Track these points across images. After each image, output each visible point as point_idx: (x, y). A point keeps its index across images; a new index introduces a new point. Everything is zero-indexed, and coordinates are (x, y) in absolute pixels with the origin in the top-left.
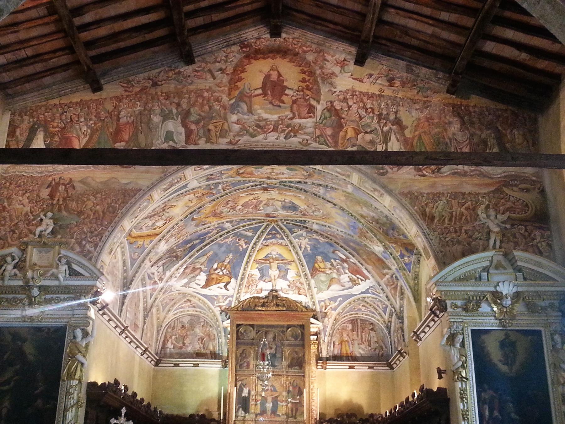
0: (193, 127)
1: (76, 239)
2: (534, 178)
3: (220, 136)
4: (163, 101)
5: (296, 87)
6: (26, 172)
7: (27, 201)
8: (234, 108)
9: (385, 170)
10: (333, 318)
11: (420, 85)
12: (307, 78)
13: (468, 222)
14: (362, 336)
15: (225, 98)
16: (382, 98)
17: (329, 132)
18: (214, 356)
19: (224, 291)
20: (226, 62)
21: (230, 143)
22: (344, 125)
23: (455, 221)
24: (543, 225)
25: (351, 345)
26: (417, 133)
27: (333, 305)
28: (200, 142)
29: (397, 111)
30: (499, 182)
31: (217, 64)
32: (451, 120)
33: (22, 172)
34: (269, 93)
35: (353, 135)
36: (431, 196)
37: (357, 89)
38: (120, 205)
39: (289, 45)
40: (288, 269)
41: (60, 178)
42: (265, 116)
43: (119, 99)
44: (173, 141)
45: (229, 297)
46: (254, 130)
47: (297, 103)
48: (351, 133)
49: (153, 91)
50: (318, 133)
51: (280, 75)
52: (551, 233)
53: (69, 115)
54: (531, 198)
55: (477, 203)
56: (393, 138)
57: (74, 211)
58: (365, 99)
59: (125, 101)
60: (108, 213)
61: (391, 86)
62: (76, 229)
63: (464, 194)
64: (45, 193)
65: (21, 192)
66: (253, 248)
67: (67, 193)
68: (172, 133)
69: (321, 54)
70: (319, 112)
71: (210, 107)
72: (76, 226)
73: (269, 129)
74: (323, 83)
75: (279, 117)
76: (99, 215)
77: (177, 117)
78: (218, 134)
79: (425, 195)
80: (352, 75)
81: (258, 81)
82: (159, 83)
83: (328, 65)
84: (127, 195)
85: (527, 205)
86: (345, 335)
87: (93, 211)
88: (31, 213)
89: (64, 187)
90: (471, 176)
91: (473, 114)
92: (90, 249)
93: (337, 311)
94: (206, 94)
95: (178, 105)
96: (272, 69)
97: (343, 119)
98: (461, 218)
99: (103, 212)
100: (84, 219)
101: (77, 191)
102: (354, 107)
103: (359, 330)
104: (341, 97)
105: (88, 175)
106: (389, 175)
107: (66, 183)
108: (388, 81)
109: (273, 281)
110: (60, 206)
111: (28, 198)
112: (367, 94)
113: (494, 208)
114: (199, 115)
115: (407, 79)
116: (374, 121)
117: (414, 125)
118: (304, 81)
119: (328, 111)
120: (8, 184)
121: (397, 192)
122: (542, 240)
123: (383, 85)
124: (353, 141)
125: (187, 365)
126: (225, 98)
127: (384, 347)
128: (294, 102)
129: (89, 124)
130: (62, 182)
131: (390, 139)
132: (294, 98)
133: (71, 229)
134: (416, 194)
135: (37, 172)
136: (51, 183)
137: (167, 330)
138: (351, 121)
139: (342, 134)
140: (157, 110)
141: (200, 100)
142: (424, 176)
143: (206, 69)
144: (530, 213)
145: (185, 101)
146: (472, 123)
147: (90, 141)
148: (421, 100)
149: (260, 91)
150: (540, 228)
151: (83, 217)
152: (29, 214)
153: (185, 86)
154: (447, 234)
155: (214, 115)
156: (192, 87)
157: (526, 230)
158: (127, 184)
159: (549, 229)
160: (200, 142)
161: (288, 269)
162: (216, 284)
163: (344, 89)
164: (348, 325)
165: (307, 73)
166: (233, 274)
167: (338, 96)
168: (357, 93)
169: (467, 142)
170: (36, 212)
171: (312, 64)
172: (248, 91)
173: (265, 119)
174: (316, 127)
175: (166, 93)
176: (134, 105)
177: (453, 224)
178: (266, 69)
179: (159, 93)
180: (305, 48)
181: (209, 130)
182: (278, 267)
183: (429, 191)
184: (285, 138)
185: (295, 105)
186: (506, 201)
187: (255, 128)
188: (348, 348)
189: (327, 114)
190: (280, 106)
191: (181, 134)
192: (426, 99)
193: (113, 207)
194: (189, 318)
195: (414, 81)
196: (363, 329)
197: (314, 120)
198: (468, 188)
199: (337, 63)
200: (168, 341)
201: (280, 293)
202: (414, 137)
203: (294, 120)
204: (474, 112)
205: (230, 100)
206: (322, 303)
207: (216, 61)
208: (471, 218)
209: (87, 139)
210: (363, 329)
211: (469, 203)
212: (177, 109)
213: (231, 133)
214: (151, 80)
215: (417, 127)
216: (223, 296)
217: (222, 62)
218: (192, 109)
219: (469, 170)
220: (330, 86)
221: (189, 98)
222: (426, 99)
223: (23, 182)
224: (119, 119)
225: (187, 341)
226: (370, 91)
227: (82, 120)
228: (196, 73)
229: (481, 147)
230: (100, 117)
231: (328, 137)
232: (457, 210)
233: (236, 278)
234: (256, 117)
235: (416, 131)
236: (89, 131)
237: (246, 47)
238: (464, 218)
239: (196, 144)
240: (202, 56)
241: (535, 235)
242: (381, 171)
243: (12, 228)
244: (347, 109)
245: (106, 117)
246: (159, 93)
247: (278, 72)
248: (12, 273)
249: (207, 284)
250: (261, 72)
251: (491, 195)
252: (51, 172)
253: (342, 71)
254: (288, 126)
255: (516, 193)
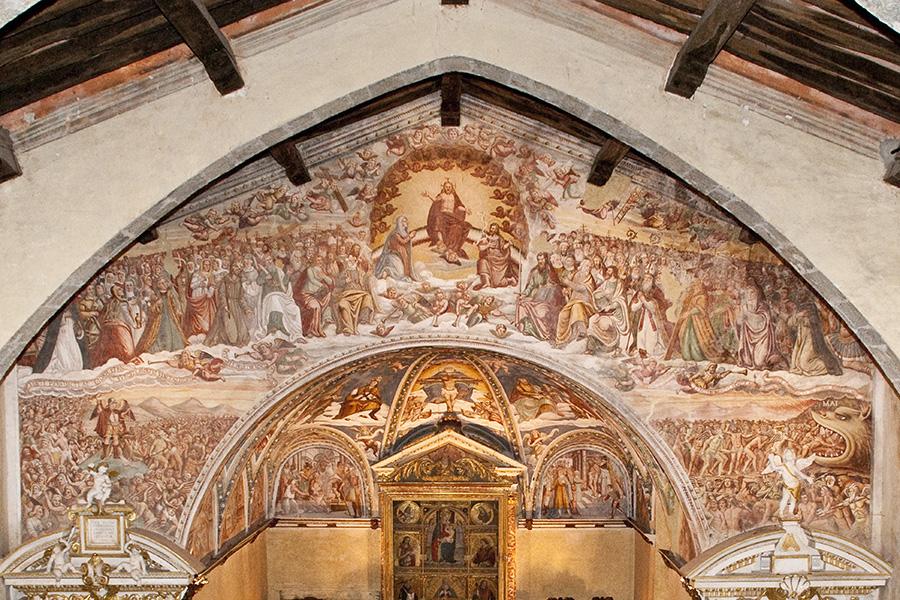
0: (314, 304)
1: (147, 503)
2: (859, 397)
3: (359, 321)
4: (261, 256)
5: (486, 228)
6: (56, 392)
7: (65, 440)
8: (380, 266)
9: (630, 382)
10: (545, 453)
11: (696, 225)
12: (506, 208)
13: (752, 471)
14: (588, 476)
15: (365, 249)
16: (632, 249)
17: (541, 312)
18: (358, 511)
19: (370, 421)
20: (364, 176)
21: (378, 333)
22: (567, 298)
23: (734, 468)
24: (862, 475)
25: (570, 491)
26: (686, 314)
27: (544, 437)
28: (327, 331)
29: (656, 274)
30: (808, 403)
31: (349, 181)
32: (742, 291)
33: (49, 391)
34: (440, 236)
35: (582, 318)
36: (700, 427)
37: (590, 230)
38: (207, 446)
39: (474, 142)
40: (473, 389)
41: (110, 400)
42: (435, 282)
43: (185, 253)
44: (282, 330)
45: (378, 428)
46: (417, 309)
47: (489, 256)
48: (577, 314)
49: (241, 236)
50: (523, 314)
51: (458, 203)
52: (872, 487)
53: (108, 285)
54: (851, 430)
55: (769, 438)
56: (647, 322)
57: (138, 456)
58: (603, 250)
59: (197, 257)
60: (190, 459)
61: (648, 225)
62: (145, 485)
63: (751, 423)
64: (90, 427)
65: (53, 426)
66: (415, 368)
67: (124, 426)
68: (279, 315)
69: (530, 160)
70: (524, 275)
71: (340, 265)
72: (145, 481)
73: (441, 307)
74: (533, 218)
75: (458, 284)
76: (177, 463)
77: (287, 286)
78: (356, 316)
79: (691, 426)
80: (582, 203)
81: (420, 214)
82: (252, 220)
83: (542, 182)
84: (216, 428)
85: (843, 443)
86: (562, 476)
87: (168, 456)
88: (75, 460)
89: (117, 416)
90: (765, 392)
91: (779, 281)
92: (171, 518)
93: (551, 446)
94: (332, 241)
95: (287, 262)
96: (444, 191)
97: (566, 287)
98: (743, 464)
99: (183, 456)
100: (155, 469)
101: (138, 422)
102: (585, 266)
103: (584, 468)
104: (564, 245)
105: (150, 395)
106: (637, 390)
107: (120, 409)
108: (644, 215)
109: (449, 402)
110: (115, 448)
111: (66, 435)
112: (608, 240)
113: (794, 447)
114: (323, 281)
115: (675, 213)
116: (617, 292)
117: (683, 298)
118: (499, 213)
119: (541, 272)
120: (32, 412)
121: (647, 420)
122: (858, 498)
123: (636, 224)
124: (582, 328)
125: (318, 530)
126: (365, 249)
127: (621, 493)
128: (483, 255)
129: (143, 302)
130: (112, 407)
131: (641, 326)
132: (483, 248)
133: (137, 486)
134: (677, 424)
135: (72, 391)
136: (97, 409)
137: (283, 470)
138: (579, 291)
139: (562, 315)
140: (252, 273)
141: (323, 254)
142: (691, 392)
143: (330, 192)
144: (844, 457)
145: (298, 253)
146: (776, 297)
147: (148, 333)
148: (696, 254)
149: (424, 234)
150: (859, 479)
151: (153, 465)
152: (73, 462)
153: (297, 224)
154: (720, 489)
155: (348, 280)
156: (307, 227)
157: (836, 484)
158: (216, 408)
159: (869, 481)
160: (327, 331)
161: (473, 389)
162: (357, 411)
163: (568, 231)
164: (567, 460)
165: (505, 198)
166: (384, 397)
167: (559, 243)
168: (591, 238)
169: (764, 333)
170: (81, 458)
171: (514, 180)
172: (404, 234)
173: (435, 289)
174: (519, 302)
175: (264, 239)
176: (212, 266)
177: (729, 473)
178: (435, 190)
179: (254, 241)
180: (501, 148)
181: (341, 310)
182: (456, 386)
183: (698, 420)
184: (468, 324)
185: (484, 261)
186: (813, 435)
187: (418, 305)
188: (566, 497)
189: (539, 279)
190: (459, 263)
191: (294, 317)
192: (704, 252)
193: (196, 449)
194: (317, 452)
195: (687, 216)
196: (591, 466)
197: (516, 289)
198: (758, 414)
199: (558, 177)
200: (286, 487)
201: (460, 416)
202: (679, 325)
203: (482, 290)
204: (782, 277)
205: (374, 251)
206: (528, 435)
207: (346, 176)
208: (757, 463)
209: (142, 329)
210: (591, 466)
211: (758, 439)
212: (285, 270)
213: (378, 315)
214: (237, 214)
215: (687, 304)
216: (369, 427)
217: (358, 176)
218: (310, 271)
219: (763, 383)
220: (544, 223)
221: (305, 248)
222: (704, 252)
223: (55, 408)
224: (190, 291)
225: (316, 488)
226: (612, 236)
227: (131, 294)
228: (313, 200)
229: (786, 341)
230: (159, 289)
231: (540, 322)
232: (738, 450)
233: (389, 405)
234: (419, 285)
235: (684, 310)
236: (144, 315)
237: (398, 145)
238: (747, 463)
239: (321, 336)
240: (323, 166)
241: (848, 491)
242: (624, 383)
243: (50, 485)
244: (572, 268)
245: (169, 288)
246: (254, 241)
247: (456, 196)
248: (65, 570)
249: (343, 414)
250: (425, 195)
251: (793, 425)
252: (94, 390)
253: (567, 195)
254: (473, 301)
255: (832, 423)
